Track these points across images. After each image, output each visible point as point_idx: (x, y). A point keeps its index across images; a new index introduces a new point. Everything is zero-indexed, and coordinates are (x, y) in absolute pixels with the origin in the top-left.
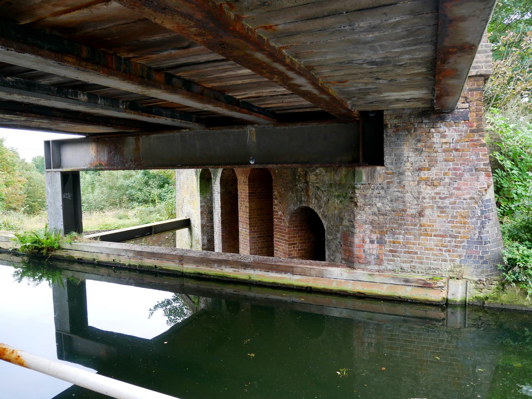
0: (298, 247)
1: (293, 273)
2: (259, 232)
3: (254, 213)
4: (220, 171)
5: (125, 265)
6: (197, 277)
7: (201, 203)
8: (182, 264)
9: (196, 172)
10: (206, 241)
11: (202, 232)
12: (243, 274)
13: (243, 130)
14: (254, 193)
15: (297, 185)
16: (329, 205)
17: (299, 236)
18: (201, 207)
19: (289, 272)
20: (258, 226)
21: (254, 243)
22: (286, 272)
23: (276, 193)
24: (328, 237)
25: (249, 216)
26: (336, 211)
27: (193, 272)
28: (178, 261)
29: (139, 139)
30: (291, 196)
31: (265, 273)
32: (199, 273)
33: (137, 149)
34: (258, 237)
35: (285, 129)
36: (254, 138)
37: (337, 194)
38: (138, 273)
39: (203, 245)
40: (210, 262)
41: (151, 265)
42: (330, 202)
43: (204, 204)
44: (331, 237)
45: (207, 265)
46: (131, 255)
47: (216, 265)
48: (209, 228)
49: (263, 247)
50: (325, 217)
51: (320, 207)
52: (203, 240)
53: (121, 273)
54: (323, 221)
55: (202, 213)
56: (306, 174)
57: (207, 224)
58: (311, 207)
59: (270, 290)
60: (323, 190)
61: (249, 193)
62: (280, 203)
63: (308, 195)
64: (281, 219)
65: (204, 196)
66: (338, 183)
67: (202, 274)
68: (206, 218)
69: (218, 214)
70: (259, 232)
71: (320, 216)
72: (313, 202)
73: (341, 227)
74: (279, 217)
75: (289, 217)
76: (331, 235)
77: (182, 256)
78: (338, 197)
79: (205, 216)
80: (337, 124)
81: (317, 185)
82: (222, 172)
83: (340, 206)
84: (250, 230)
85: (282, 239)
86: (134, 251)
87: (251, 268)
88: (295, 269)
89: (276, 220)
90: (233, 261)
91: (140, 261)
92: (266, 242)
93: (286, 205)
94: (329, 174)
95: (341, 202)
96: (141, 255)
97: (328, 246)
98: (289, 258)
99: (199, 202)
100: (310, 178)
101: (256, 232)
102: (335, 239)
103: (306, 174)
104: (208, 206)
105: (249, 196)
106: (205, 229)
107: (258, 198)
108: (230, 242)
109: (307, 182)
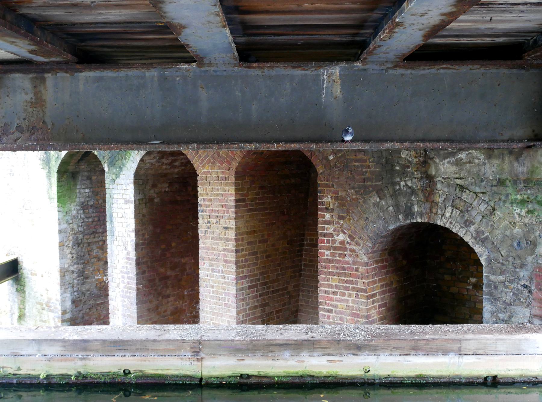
0: (378, 301)
1: (460, 353)
2: (249, 276)
3: (242, 240)
4: (133, 159)
5: (37, 377)
6: (239, 383)
7: (60, 224)
8: (200, 360)
9: (47, 162)
10: (68, 304)
11: (63, 284)
12: (349, 366)
13: (315, 73)
14: (244, 200)
15: (399, 183)
16: (496, 219)
17: (380, 280)
18: (60, 232)
19: (452, 351)
20: (249, 267)
21: (243, 299)
22: (445, 353)
23: (327, 199)
24: (492, 277)
25: (237, 246)
26: (517, 230)
27: (229, 373)
28: (189, 354)
29: (43, 80)
30: (376, 205)
31: (402, 358)
32: (241, 376)
33: (38, 102)
34: (250, 287)
35: (402, 75)
36: (337, 90)
37: (519, 197)
38: (73, 394)
39: (64, 312)
40: (272, 348)
41: (116, 370)
42: (496, 212)
43: (65, 226)
44: (502, 278)
45: (265, 356)
46: (53, 350)
47: (287, 353)
48: (75, 275)
49: (256, 307)
50: (484, 241)
51: (468, 224)
52: (63, 301)
53: (20, 397)
54: (478, 249)
55: (61, 245)
56: (425, 162)
57: (72, 268)
58: (440, 223)
59: (411, 391)
60: (477, 190)
61: (237, 201)
62: (341, 218)
63: (434, 204)
64: (345, 249)
65: (66, 209)
66: (522, 177)
67: (249, 376)
68: (69, 256)
69: (125, 245)
70: (249, 276)
71: (468, 239)
72: (448, 215)
73: (530, 259)
74: (337, 245)
75: (369, 244)
76: (502, 273)
77: (199, 342)
78: (523, 203)
79: (68, 251)
80: (506, 71)
81: (458, 182)
82: (142, 160)
83: (527, 220)
84: (237, 273)
85: (347, 288)
86: (63, 341)
87: (370, 351)
88: (464, 345)
89: (327, 252)
90: (329, 342)
91: (80, 363)
92: (260, 296)
93: (363, 222)
94: (496, 162)
95: (529, 212)
96: (85, 349)
97: (490, 294)
98: (366, 323)
99: (57, 222)
100: (437, 170)
101: (245, 277)
102: (511, 282)
103: (425, 163)
104: (73, 230)
105: (236, 207)
106: (67, 278)
107: (250, 210)
108: (151, 302)
109: (430, 178)
